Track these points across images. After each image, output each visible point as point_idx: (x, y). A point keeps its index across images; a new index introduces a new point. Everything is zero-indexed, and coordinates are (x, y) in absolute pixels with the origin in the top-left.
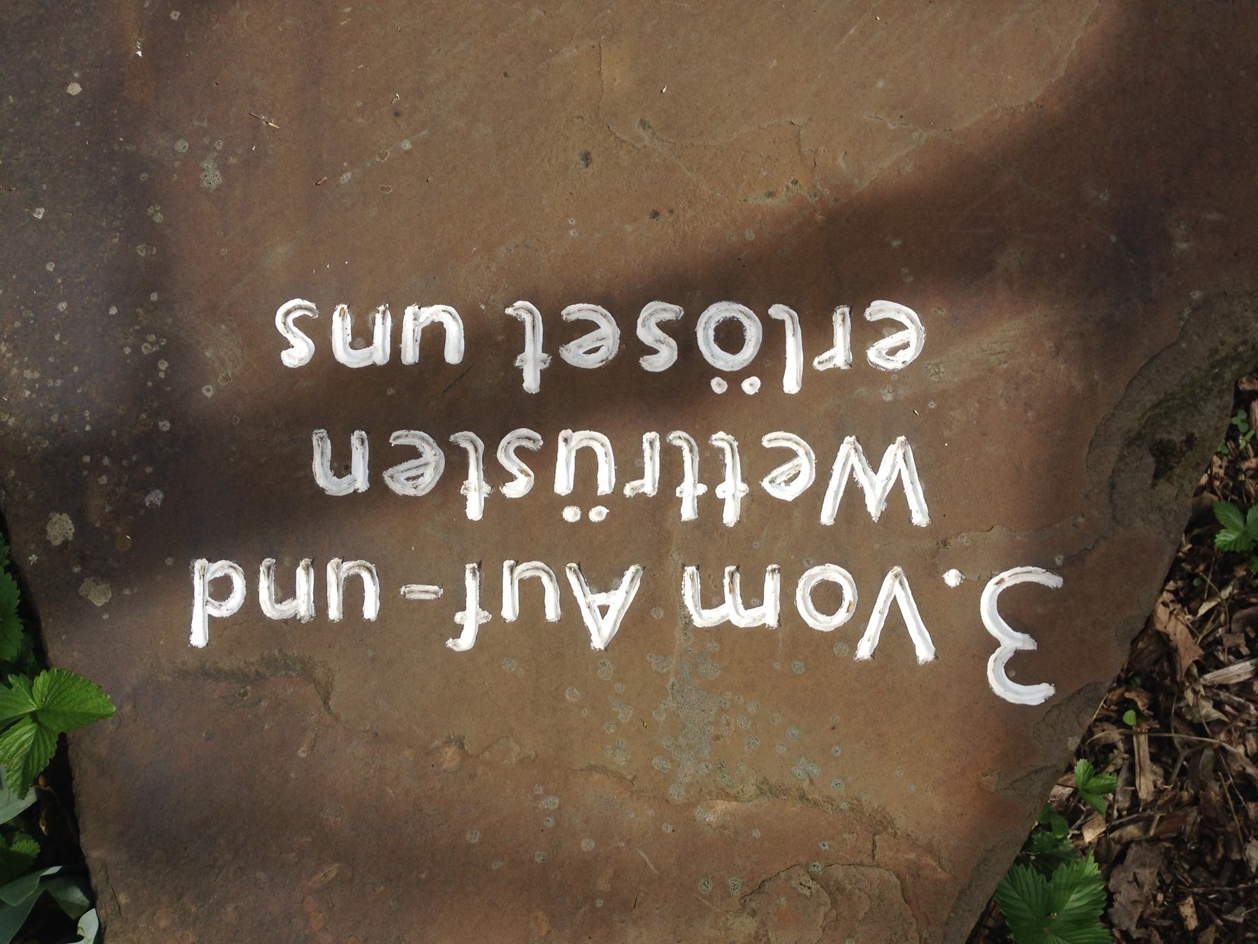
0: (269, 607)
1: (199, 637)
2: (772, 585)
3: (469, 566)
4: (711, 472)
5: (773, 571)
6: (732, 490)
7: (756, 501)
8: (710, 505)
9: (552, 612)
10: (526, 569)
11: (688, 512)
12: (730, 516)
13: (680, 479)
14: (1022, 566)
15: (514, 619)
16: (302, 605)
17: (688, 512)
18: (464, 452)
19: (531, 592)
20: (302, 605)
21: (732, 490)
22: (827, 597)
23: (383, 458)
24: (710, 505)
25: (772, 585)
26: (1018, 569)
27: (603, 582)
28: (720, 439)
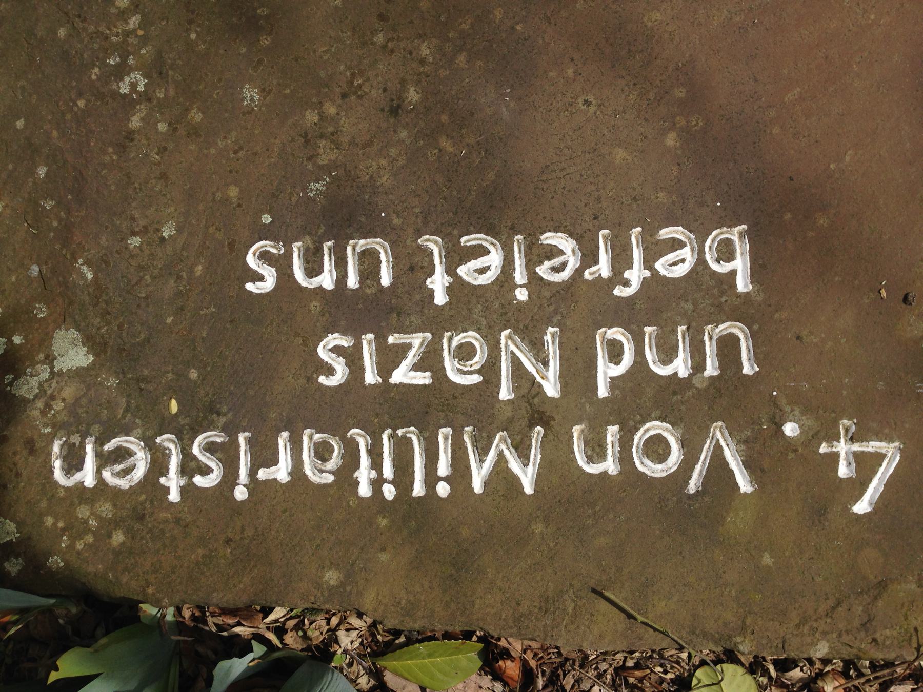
7: (457, 288)
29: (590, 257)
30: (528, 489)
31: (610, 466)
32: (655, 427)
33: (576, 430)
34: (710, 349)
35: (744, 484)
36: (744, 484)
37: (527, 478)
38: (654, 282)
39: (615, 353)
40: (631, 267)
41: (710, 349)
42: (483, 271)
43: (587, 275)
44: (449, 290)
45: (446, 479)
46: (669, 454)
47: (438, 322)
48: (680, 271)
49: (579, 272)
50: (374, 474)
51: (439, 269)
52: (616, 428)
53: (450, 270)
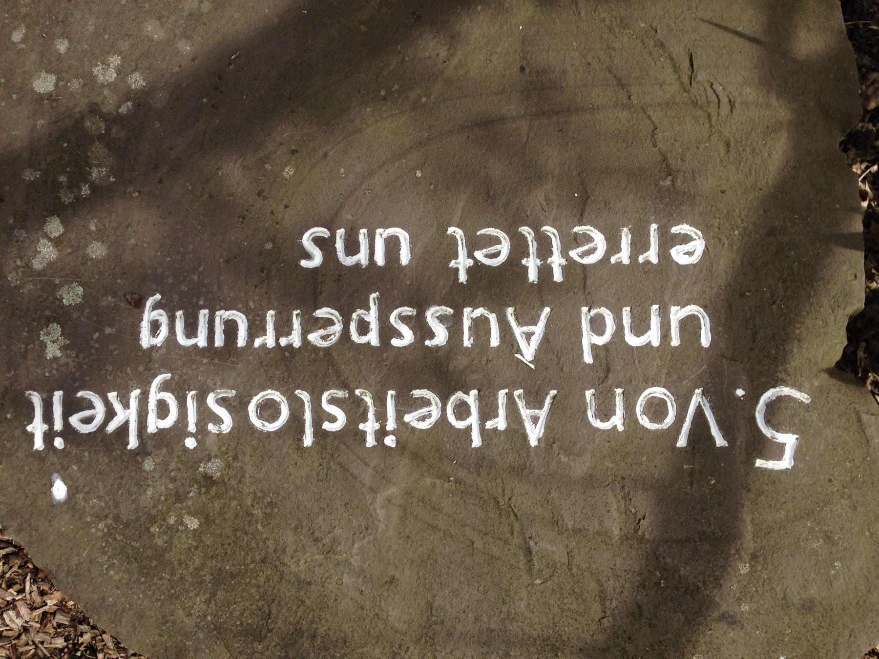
0: (182, 340)
1: (588, 359)
2: (655, 322)
3: (295, 313)
4: (545, 250)
5: (297, 315)
6: (556, 261)
7: (570, 267)
8: (545, 271)
9: (495, 341)
10: (479, 311)
11: (532, 276)
12: (558, 277)
13: (551, 253)
14: (143, 312)
15: (498, 344)
16: (653, 337)
17: (532, 276)
18: (525, 239)
19: (480, 327)
20: (653, 337)
21: (556, 261)
22: (656, 409)
23: (668, 241)
24: (545, 271)
25: (655, 322)
26: (702, 310)
27: (527, 318)
28: (525, 230)
29: (613, 246)
30: (533, 443)
31: (617, 421)
32: (658, 392)
33: (589, 393)
34: (219, 328)
35: (720, 441)
36: (720, 441)
37: (534, 434)
38: (477, 269)
39: (155, 327)
40: (456, 257)
41: (219, 328)
42: (690, 254)
43: (613, 260)
44: (469, 271)
45: (392, 433)
46: (280, 413)
47: (458, 297)
48: (694, 259)
49: (606, 259)
50: (46, 427)
51: (462, 252)
52: (61, 393)
53: (564, 253)
